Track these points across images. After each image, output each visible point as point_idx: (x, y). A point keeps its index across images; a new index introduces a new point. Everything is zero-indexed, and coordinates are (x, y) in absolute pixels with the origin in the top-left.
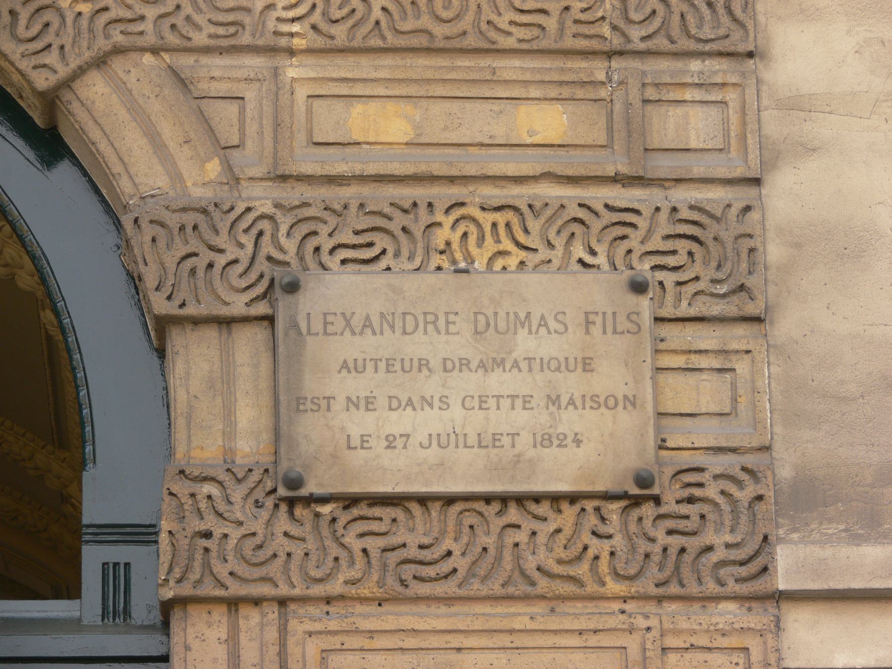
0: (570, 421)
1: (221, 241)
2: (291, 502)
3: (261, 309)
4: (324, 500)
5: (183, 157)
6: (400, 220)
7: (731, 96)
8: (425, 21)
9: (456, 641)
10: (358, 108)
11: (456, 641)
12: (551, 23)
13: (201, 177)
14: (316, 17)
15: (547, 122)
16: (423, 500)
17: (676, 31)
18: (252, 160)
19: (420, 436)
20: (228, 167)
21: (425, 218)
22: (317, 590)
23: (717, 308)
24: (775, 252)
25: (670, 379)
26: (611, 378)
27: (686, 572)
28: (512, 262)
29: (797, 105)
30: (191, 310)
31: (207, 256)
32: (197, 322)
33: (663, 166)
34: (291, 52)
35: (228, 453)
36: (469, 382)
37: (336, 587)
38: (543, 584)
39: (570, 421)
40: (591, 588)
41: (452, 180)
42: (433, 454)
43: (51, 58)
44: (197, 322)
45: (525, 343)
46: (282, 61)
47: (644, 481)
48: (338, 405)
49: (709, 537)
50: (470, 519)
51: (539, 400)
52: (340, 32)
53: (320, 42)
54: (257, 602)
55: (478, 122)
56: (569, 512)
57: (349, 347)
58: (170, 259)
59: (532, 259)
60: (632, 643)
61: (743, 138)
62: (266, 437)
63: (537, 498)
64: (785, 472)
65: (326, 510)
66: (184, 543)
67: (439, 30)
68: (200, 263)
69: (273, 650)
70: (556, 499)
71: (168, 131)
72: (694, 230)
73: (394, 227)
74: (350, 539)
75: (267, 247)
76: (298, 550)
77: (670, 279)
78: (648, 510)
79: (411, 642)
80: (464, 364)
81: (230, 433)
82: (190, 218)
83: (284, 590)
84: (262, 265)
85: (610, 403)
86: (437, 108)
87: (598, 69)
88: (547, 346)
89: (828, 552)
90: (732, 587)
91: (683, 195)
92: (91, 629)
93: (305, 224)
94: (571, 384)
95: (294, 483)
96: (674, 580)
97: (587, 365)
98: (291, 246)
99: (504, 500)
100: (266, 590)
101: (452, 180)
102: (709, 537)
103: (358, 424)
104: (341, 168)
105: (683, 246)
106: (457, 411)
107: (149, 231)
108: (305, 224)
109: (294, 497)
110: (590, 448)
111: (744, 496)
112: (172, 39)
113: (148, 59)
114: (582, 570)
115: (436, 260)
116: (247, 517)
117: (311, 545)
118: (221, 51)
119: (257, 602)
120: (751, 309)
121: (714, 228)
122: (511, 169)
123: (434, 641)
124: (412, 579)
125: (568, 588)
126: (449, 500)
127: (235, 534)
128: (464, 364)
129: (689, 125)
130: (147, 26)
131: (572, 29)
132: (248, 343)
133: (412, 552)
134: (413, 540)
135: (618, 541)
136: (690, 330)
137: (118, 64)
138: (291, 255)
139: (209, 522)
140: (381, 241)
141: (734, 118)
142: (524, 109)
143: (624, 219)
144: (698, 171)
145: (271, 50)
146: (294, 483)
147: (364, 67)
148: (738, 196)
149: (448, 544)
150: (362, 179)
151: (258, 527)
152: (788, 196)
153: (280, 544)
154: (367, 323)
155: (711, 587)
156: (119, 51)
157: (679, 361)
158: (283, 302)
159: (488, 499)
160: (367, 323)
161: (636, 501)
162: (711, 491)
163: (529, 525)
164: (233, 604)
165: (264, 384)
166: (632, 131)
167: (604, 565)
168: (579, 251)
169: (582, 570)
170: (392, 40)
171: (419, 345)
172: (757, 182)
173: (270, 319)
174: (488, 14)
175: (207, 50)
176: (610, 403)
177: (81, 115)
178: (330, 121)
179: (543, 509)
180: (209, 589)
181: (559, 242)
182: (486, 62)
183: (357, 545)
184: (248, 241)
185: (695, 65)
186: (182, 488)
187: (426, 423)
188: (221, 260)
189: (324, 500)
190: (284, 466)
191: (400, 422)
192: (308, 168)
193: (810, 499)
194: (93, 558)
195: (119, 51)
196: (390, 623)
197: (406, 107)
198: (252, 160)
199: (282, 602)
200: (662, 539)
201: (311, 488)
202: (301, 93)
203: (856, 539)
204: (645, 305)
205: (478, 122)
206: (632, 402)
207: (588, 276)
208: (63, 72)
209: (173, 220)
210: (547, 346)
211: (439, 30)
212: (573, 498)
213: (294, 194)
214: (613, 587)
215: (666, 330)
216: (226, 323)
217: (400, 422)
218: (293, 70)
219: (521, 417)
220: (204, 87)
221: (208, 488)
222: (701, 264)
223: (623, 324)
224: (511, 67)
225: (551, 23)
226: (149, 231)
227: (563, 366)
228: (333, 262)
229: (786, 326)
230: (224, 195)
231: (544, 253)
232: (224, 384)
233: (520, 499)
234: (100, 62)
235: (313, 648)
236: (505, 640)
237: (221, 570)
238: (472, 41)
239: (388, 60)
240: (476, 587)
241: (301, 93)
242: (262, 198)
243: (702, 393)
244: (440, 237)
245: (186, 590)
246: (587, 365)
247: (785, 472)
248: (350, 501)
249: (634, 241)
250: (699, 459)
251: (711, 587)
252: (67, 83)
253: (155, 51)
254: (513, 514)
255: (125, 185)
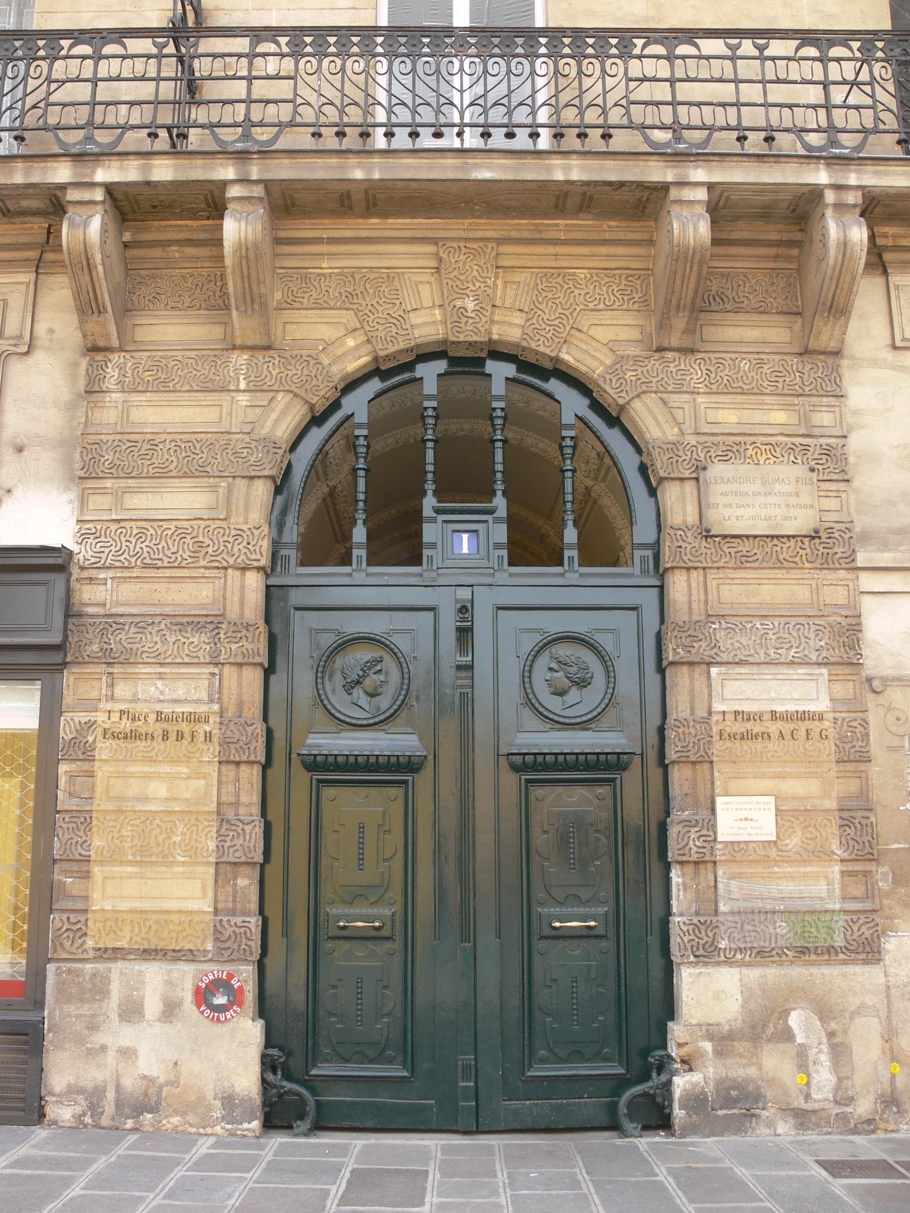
0: (793, 512)
1: (680, 453)
2: (706, 537)
3: (694, 475)
4: (716, 536)
5: (665, 426)
6: (736, 448)
7: (837, 409)
8: (741, 384)
9: (759, 581)
10: (721, 411)
11: (759, 581)
12: (780, 385)
13: (672, 433)
14: (706, 382)
15: (780, 417)
16: (747, 537)
17: (819, 388)
18: (688, 428)
19: (747, 516)
20: (681, 430)
21: (743, 447)
22: (715, 565)
23: (835, 477)
24: (852, 459)
25: (822, 499)
26: (805, 499)
27: (830, 561)
28: (772, 461)
29: (856, 413)
30: (672, 475)
31: (676, 458)
32: (673, 479)
33: (817, 431)
34: (698, 393)
35: (685, 521)
36: (762, 499)
37: (721, 564)
38: (785, 564)
39: (793, 512)
40: (800, 565)
41: (751, 435)
42: (751, 522)
43: (624, 394)
44: (673, 479)
45: (778, 487)
46: (695, 396)
47: (816, 531)
48: (721, 506)
49: (836, 550)
50: (762, 543)
51: (783, 506)
52: (714, 387)
53: (708, 390)
54: (696, 568)
55: (758, 417)
56: (793, 541)
57: (723, 488)
58: (665, 459)
59: (778, 461)
60: (813, 583)
61: (841, 423)
62: (697, 516)
63: (783, 537)
64: (858, 529)
65: (717, 539)
66: (673, 549)
67: (745, 387)
68: (674, 460)
69: (701, 584)
70: (788, 537)
71: (661, 419)
72: (827, 452)
73: (734, 450)
74: (725, 549)
75: (695, 456)
76: (709, 552)
77: (820, 467)
78: (817, 541)
79: (745, 582)
80: (759, 494)
81: (685, 515)
82: (670, 446)
83: (705, 565)
84: (693, 461)
85: (805, 507)
86: (745, 412)
87: (795, 400)
88: (785, 488)
89: (873, 555)
90: (844, 565)
91: (823, 441)
92: (637, 577)
93: (707, 448)
94: (793, 500)
95: (708, 531)
96: (827, 563)
97: (797, 495)
98: (702, 455)
99: (772, 537)
100: (699, 565)
101: (751, 435)
102: (836, 550)
103: (727, 512)
104: (716, 431)
105: (824, 457)
106: (757, 509)
107: (657, 450)
108: (707, 448)
109: (707, 535)
110: (799, 521)
111: (847, 536)
112: (661, 389)
113: (653, 395)
114: (797, 559)
115: (748, 460)
116: (693, 542)
117: (713, 550)
118: (676, 393)
119: (696, 568)
120: (846, 477)
121: (834, 452)
122: (770, 432)
123: (752, 581)
124: (744, 562)
125: (793, 565)
126: (755, 537)
127: (689, 547)
128: (759, 494)
129: (824, 419)
130: (653, 384)
131: (786, 387)
132: (690, 486)
133: (744, 553)
134: (745, 550)
135: (808, 550)
136: (827, 484)
137: (643, 396)
138: (702, 459)
139: (681, 543)
140: (730, 454)
141: (838, 417)
142: (772, 412)
143: (806, 448)
144: (828, 433)
145: (692, 393)
146: (708, 531)
147: (722, 398)
148: (841, 441)
149: (755, 551)
150: (723, 434)
151: (696, 544)
152: (855, 442)
153: (703, 550)
154: (728, 480)
155: (837, 566)
156: (644, 392)
157: (824, 494)
158: (702, 473)
159: (767, 536)
160: (728, 480)
161: (813, 538)
162: (836, 535)
163: (780, 545)
164: (688, 569)
165: (696, 499)
166: (805, 419)
167: (804, 558)
168: (792, 458)
169: (797, 559)
170: (730, 390)
171: (744, 488)
172: (846, 437)
173: (697, 479)
174: (760, 382)
175: (672, 392)
176: (805, 507)
177: (633, 413)
178: (712, 416)
179: (785, 540)
180: (682, 564)
181: (786, 455)
182: (760, 397)
183: (727, 551)
184: (689, 453)
185: (825, 399)
186: (672, 532)
187: (748, 512)
188: (680, 460)
189: (716, 536)
190: (704, 525)
191: (740, 512)
192: (707, 431)
193: (866, 538)
194: (426, 552)
195: (644, 392)
196: (738, 576)
197: (736, 412)
198: (688, 428)
199: (704, 569)
200: (822, 550)
201: (713, 532)
202: (703, 406)
203: (881, 551)
204: (814, 475)
205: (758, 417)
206: (812, 506)
207: (796, 466)
208: (627, 399)
209: (665, 447)
210: (785, 488)
211: (745, 387)
212: (794, 537)
213: (702, 439)
214: (807, 565)
215: (820, 484)
216: (682, 480)
217: (740, 512)
218: (700, 399)
219: (778, 511)
220: (671, 404)
221: (680, 532)
222: (830, 463)
223: (808, 482)
224: (768, 399)
225: (780, 385)
226: (657, 450)
227: (790, 495)
228: (716, 461)
229: (856, 483)
230: (679, 438)
231: (781, 459)
232: (682, 499)
233: (777, 537)
234: (638, 396)
235: (715, 583)
236: (774, 581)
237: (685, 558)
238: (756, 391)
239: (729, 396)
240: (765, 565)
241: (703, 406)
242: (693, 440)
243: (833, 504)
244: (749, 453)
245: (674, 564)
246: (797, 495)
247: (858, 529)
248: (725, 537)
249: (809, 454)
250: (832, 525)
251: (837, 566)
252: (628, 403)
253: (655, 392)
254: (775, 541)
255: (648, 435)
